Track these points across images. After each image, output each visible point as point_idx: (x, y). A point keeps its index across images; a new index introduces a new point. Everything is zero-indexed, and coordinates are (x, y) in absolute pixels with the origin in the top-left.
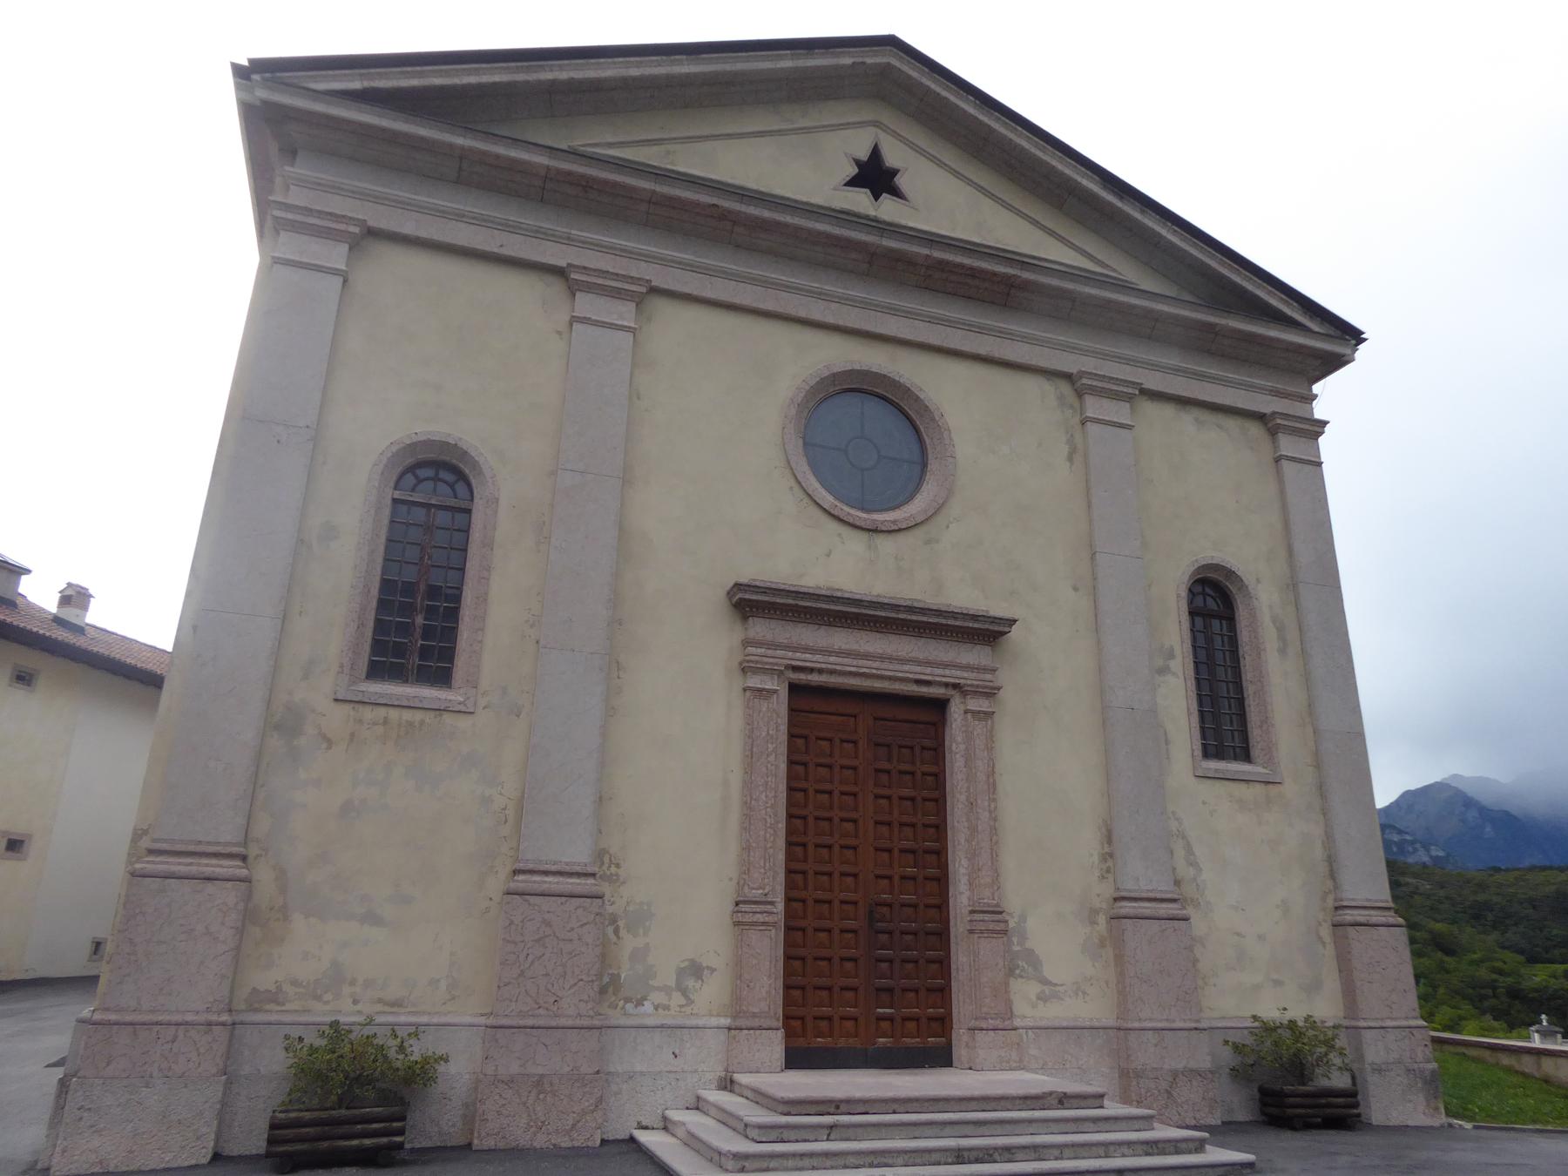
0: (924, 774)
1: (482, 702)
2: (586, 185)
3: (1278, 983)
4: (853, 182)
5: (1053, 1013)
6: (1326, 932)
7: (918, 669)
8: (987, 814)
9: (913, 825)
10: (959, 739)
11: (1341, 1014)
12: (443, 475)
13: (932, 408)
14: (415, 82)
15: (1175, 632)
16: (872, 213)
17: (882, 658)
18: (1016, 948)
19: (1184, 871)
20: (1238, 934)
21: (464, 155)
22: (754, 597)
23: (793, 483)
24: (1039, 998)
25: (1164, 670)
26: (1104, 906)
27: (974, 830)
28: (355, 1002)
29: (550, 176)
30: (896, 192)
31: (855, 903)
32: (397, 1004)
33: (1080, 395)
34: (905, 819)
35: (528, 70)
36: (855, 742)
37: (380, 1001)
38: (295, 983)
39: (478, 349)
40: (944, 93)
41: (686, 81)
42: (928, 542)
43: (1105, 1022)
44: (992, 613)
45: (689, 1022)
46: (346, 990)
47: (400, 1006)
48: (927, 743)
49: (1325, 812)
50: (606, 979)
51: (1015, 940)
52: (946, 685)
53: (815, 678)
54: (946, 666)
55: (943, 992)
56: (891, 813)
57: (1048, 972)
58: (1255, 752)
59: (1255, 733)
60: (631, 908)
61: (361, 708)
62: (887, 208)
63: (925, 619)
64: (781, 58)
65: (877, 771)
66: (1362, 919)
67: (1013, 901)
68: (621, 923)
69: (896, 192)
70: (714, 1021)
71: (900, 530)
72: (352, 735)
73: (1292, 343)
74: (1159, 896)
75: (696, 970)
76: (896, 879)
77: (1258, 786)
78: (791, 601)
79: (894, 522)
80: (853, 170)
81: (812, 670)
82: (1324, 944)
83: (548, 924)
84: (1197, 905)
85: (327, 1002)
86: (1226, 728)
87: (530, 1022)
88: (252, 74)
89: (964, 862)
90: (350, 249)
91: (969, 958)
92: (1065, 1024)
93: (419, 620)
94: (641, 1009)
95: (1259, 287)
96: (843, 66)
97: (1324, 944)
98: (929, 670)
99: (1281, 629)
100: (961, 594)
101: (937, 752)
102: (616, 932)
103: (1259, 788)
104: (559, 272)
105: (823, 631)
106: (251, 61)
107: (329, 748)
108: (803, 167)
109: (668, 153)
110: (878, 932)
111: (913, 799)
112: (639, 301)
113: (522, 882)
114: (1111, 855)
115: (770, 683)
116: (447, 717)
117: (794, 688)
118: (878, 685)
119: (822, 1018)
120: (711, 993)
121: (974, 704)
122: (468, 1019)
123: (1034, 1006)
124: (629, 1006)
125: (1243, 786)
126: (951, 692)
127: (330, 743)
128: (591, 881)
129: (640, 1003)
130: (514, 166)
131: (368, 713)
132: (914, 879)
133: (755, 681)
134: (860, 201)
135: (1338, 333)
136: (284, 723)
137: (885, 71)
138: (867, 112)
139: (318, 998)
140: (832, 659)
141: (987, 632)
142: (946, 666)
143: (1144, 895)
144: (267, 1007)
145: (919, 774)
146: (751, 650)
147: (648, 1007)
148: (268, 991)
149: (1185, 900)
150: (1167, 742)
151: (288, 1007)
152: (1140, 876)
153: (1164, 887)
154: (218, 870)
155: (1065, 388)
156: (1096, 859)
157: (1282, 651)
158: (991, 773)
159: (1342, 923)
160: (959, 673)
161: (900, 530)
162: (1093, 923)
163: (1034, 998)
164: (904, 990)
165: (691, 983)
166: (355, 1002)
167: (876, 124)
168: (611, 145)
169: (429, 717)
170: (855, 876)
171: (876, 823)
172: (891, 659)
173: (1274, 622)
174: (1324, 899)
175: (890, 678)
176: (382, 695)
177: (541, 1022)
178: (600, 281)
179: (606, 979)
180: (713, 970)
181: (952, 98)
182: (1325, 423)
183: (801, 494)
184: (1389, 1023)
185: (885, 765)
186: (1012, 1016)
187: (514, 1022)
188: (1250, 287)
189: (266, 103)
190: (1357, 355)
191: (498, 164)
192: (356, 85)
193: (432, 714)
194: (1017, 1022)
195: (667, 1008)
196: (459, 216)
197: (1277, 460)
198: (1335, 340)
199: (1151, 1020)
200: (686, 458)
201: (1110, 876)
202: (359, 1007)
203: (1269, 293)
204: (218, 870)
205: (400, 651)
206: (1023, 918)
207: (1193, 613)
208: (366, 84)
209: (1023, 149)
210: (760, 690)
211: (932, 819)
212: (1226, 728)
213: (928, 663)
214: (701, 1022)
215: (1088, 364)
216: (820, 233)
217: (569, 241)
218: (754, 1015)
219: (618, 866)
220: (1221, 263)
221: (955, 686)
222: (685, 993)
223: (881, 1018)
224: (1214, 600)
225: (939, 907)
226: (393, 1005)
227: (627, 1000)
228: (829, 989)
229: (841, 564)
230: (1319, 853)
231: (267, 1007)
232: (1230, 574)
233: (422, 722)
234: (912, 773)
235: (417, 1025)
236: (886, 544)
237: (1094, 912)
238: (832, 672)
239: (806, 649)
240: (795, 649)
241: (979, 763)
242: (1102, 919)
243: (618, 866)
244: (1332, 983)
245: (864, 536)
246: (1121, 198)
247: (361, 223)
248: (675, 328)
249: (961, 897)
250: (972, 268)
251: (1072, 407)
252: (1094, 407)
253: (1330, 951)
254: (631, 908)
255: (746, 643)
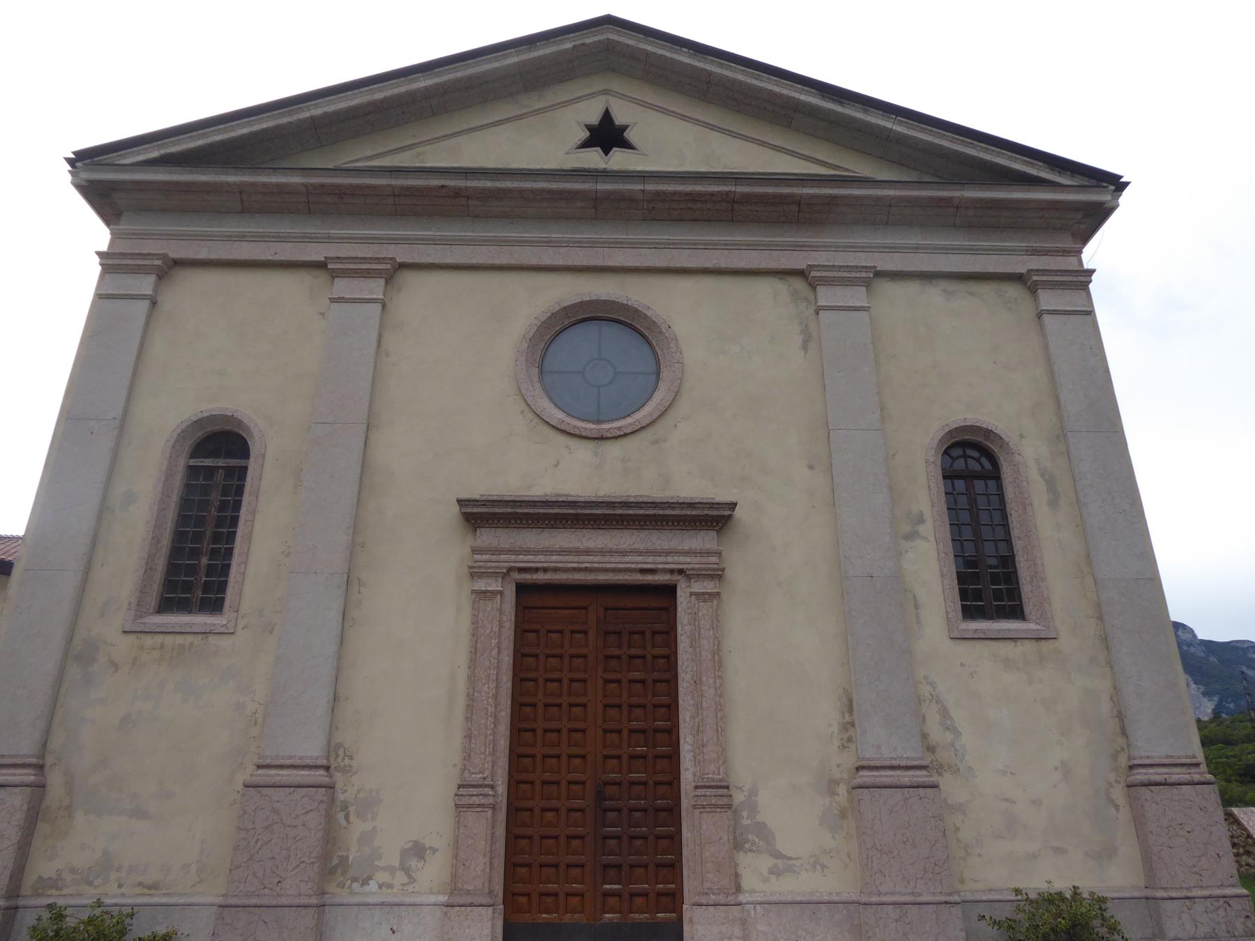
0: (655, 657)
1: (241, 623)
2: (340, 193)
3: (1060, 851)
4: (586, 144)
5: (788, 887)
6: (1118, 794)
7: (640, 559)
8: (713, 691)
9: (643, 706)
10: (685, 621)
11: (1142, 884)
12: (970, 452)
13: (659, 322)
14: (200, 143)
15: (925, 495)
16: (602, 166)
17: (602, 552)
18: (746, 822)
19: (937, 734)
20: (1007, 800)
21: (241, 189)
22: (475, 510)
23: (523, 407)
24: (771, 872)
25: (911, 536)
26: (846, 777)
27: (698, 707)
28: (120, 886)
29: (310, 190)
30: (627, 145)
31: (583, 783)
32: (154, 886)
33: (813, 288)
34: (634, 700)
35: (290, 113)
36: (585, 632)
37: (140, 884)
38: (73, 870)
39: (256, 340)
40: (660, 52)
41: (427, 94)
42: (656, 442)
43: (845, 897)
44: (718, 499)
45: (408, 900)
46: (113, 876)
47: (157, 888)
48: (658, 627)
49: (1110, 665)
50: (335, 861)
51: (745, 814)
52: (672, 571)
53: (541, 577)
54: (667, 553)
55: (674, 868)
56: (620, 696)
57: (783, 845)
58: (1028, 609)
59: (1026, 589)
60: (361, 795)
61: (143, 636)
62: (618, 160)
63: (642, 512)
64: (505, 57)
65: (606, 657)
66: (1158, 778)
67: (743, 772)
68: (352, 809)
69: (627, 145)
70: (432, 899)
71: (626, 435)
72: (135, 659)
73: (1043, 201)
74: (903, 763)
75: (419, 851)
76: (625, 758)
77: (1026, 642)
78: (510, 510)
79: (619, 428)
80: (585, 134)
81: (537, 570)
82: (1117, 807)
83: (275, 811)
84: (955, 771)
85: (96, 887)
86: (990, 586)
87: (254, 901)
88: (83, 160)
89: (689, 739)
90: (387, 283)
91: (699, 833)
92: (798, 899)
93: (205, 561)
94: (367, 888)
95: (998, 155)
96: (566, 51)
97: (1117, 807)
98: (650, 559)
99: (1051, 483)
100: (688, 485)
101: (669, 634)
102: (347, 817)
103: (1028, 646)
104: (321, 266)
105: (644, 534)
106: (74, 153)
107: (115, 672)
108: (543, 141)
109: (419, 154)
110: (606, 810)
111: (643, 682)
112: (867, 283)
113: (866, 777)
114: (853, 724)
115: (495, 585)
116: (212, 639)
117: (521, 588)
118: (602, 578)
119: (548, 895)
120: (433, 872)
121: (697, 587)
122: (210, 899)
123: (766, 880)
124: (356, 886)
125: (1010, 645)
126: (676, 577)
127: (116, 667)
128: (924, 773)
129: (365, 882)
130: (281, 189)
131: (149, 641)
132: (644, 757)
133: (481, 585)
134: (593, 158)
135: (1094, 182)
136: (77, 653)
137: (609, 46)
138: (597, 84)
139: (90, 883)
140: (554, 558)
141: (714, 518)
142: (667, 553)
143: (887, 763)
144: (49, 892)
145: (649, 657)
146: (478, 557)
147: (373, 886)
148: (50, 878)
149: (941, 766)
150: (916, 607)
151: (65, 892)
152: (885, 741)
153: (909, 752)
154: (10, 778)
155: (799, 284)
156: (835, 729)
157: (1054, 503)
158: (717, 651)
159: (1140, 781)
160: (681, 559)
161: (626, 435)
162: (833, 793)
163: (765, 872)
164: (632, 866)
165: (413, 863)
166: (120, 886)
167: (606, 92)
168: (357, 160)
169: (197, 640)
170: (583, 757)
171: (606, 706)
172: (611, 552)
173: (1042, 475)
174: (1114, 757)
175: (614, 570)
176: (159, 625)
177: (264, 901)
178: (352, 266)
179: (335, 861)
180: (434, 851)
181: (668, 54)
182: (1093, 271)
183: (530, 415)
184: (1196, 892)
185: (614, 651)
186: (738, 889)
187: (244, 901)
188: (987, 157)
189: (91, 182)
190: (1121, 200)
191: (267, 190)
192: (155, 154)
193: (200, 637)
194: (742, 898)
195: (390, 886)
196: (242, 238)
197: (1040, 316)
198: (1089, 194)
199: (892, 894)
200: (442, 397)
201: (852, 746)
202: (123, 890)
203: (1010, 158)
204: (10, 778)
205: (188, 587)
206: (754, 792)
207: (949, 476)
208: (162, 152)
209: (740, 82)
210: (484, 592)
211: (664, 699)
212: (990, 586)
213: (649, 552)
214: (418, 900)
215: (332, 251)
216: (542, 191)
217: (329, 239)
218: (468, 892)
219: (351, 758)
220: (953, 141)
221: (681, 572)
222: (407, 871)
223: (607, 894)
224: (972, 463)
225: (670, 784)
226: (150, 888)
227: (355, 880)
228: (556, 866)
229: (575, 473)
230: (1106, 708)
231: (49, 892)
232: (988, 433)
233: (192, 644)
234: (644, 657)
235: (132, 906)
236: (613, 450)
237: (833, 782)
238: (556, 570)
239: (528, 552)
240: (517, 553)
241: (704, 642)
242: (842, 790)
243: (351, 758)
244: (1128, 849)
245: (590, 445)
246: (841, 103)
247: (164, 257)
248: (419, 293)
249: (688, 774)
250: (687, 194)
251: (806, 299)
252: (826, 296)
253: (1124, 814)
254: (361, 795)
255: (475, 551)
